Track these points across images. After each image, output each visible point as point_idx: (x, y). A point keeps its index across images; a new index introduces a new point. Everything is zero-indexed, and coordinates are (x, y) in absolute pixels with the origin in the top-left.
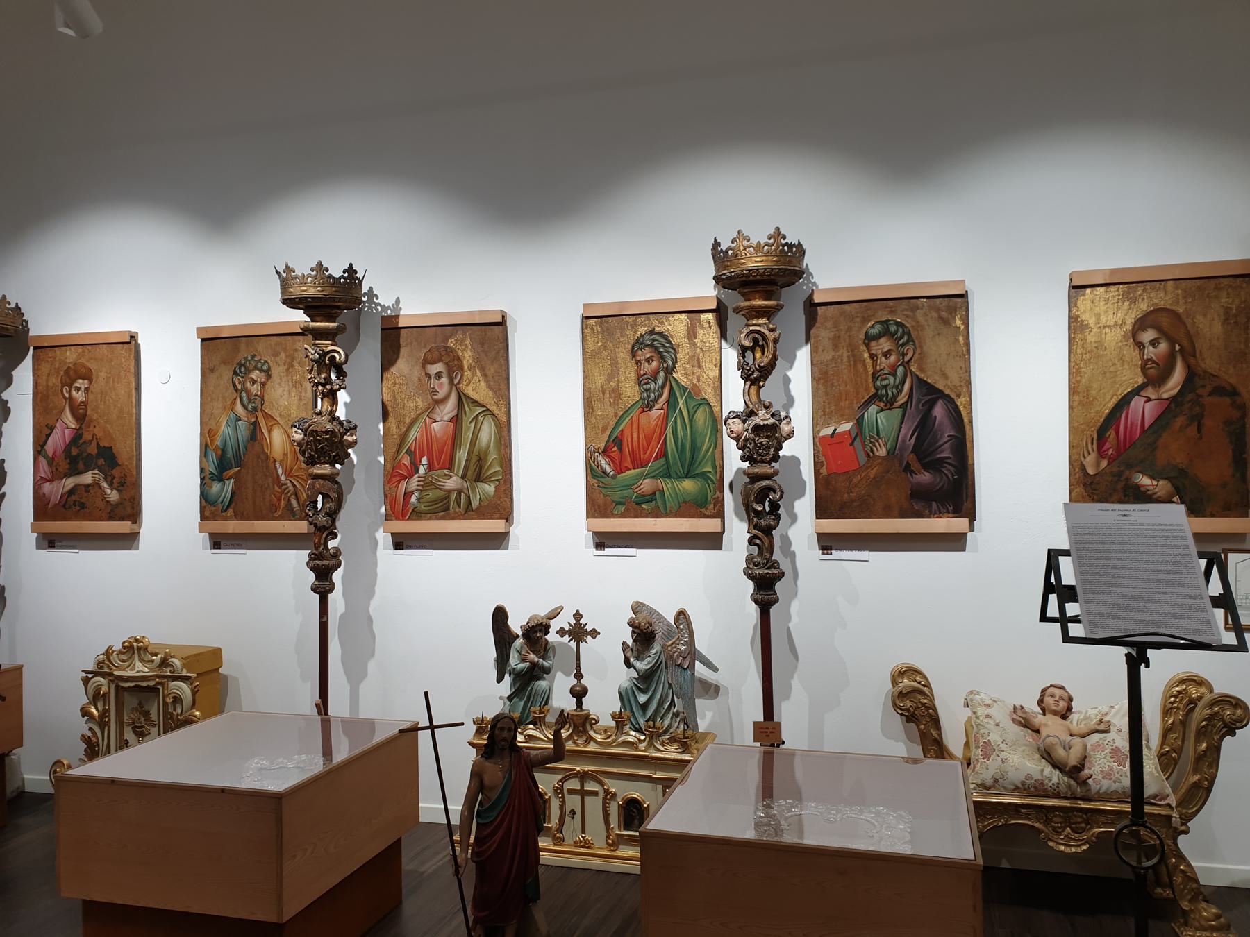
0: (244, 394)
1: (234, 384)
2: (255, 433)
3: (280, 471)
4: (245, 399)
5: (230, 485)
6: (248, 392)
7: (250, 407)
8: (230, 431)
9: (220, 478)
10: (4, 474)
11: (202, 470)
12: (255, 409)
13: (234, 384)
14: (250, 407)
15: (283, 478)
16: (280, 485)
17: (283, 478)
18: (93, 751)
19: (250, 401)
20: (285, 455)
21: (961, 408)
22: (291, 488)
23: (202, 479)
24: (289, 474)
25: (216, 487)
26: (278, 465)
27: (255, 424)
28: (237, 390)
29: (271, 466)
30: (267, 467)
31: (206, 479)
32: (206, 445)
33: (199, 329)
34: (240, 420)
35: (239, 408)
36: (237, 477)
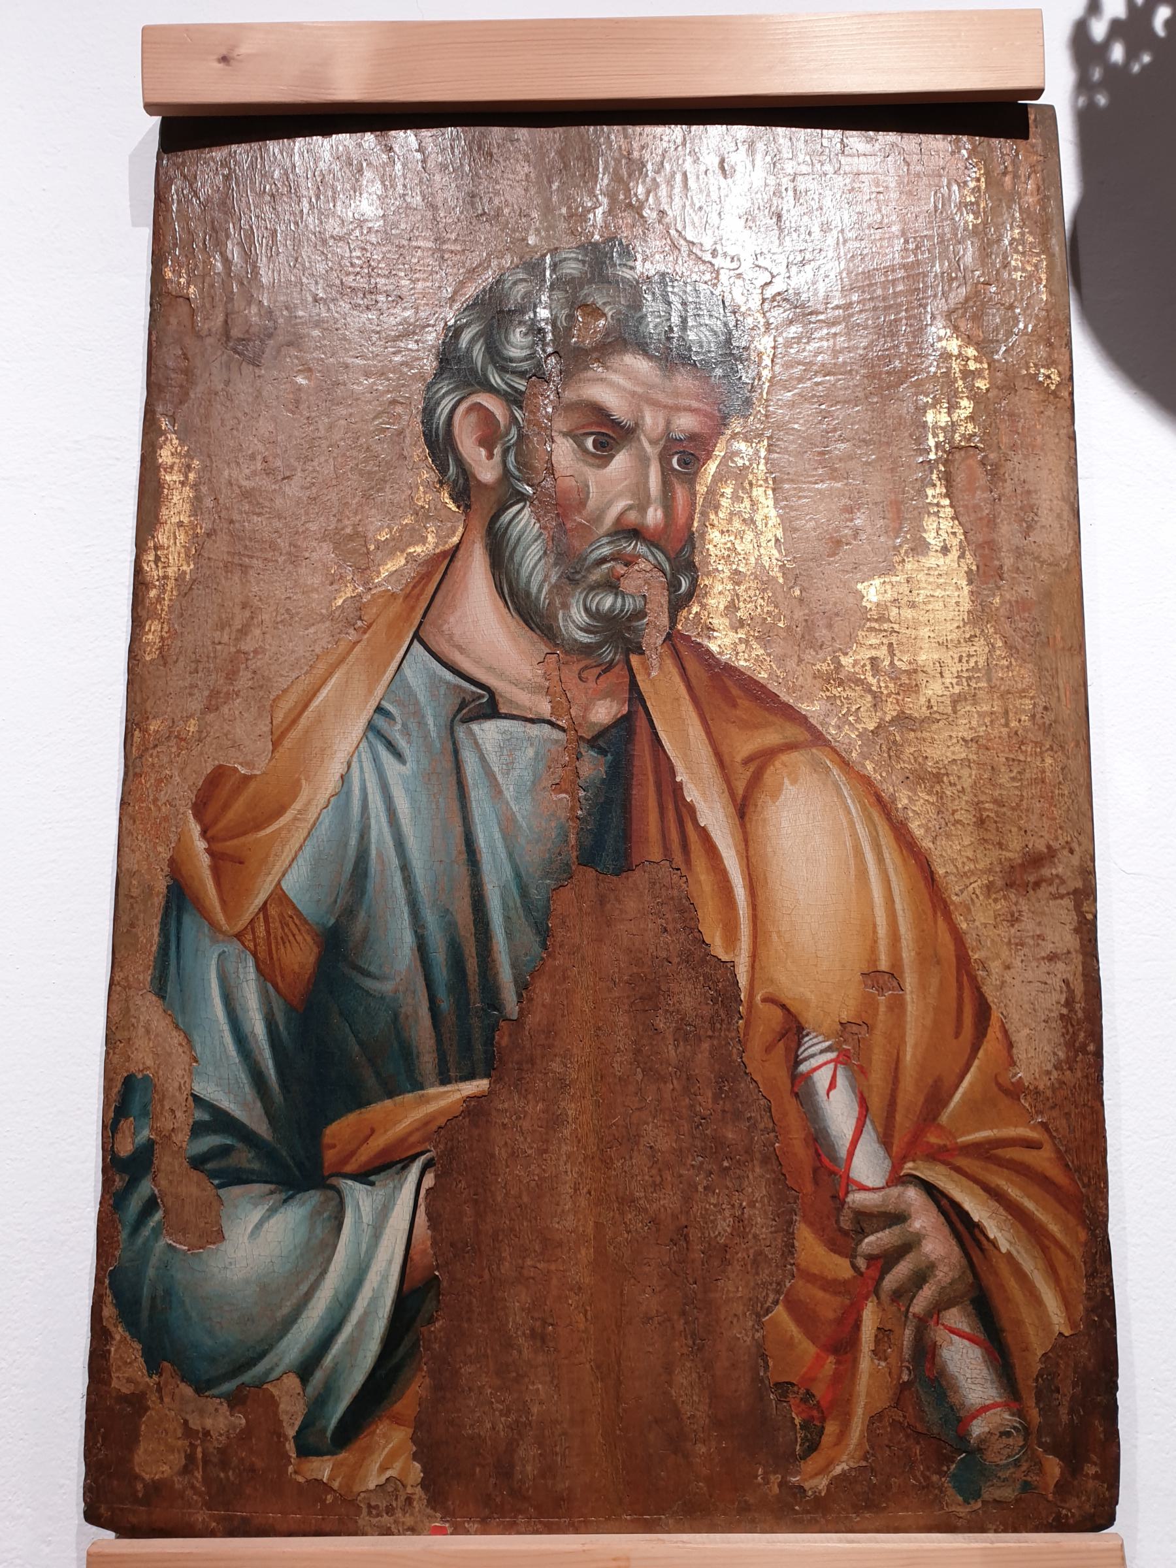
0: (524, 522)
1: (440, 445)
2: (618, 809)
3: (839, 1111)
4: (534, 564)
5: (383, 1227)
6: (561, 509)
7: (574, 620)
8: (398, 801)
9: (295, 1159)
10: (1114, 1520)
11: (125, 1097)
12: (619, 633)
13: (440, 445)
14: (574, 620)
15: (868, 1167)
16: (847, 1228)
17: (868, 1167)
18: (475, 1108)
19: (573, 571)
20: (880, 980)
21: (296, 1428)
22: (937, 1245)
23: (123, 1171)
24: (912, 1133)
25: (256, 1238)
26: (819, 1063)
27: (624, 747)
28: (464, 489)
29: (766, 1069)
30: (730, 1073)
31: (148, 1172)
32: (180, 897)
33: (158, 43)
34: (484, 705)
35: (481, 624)
36: (455, 1162)
